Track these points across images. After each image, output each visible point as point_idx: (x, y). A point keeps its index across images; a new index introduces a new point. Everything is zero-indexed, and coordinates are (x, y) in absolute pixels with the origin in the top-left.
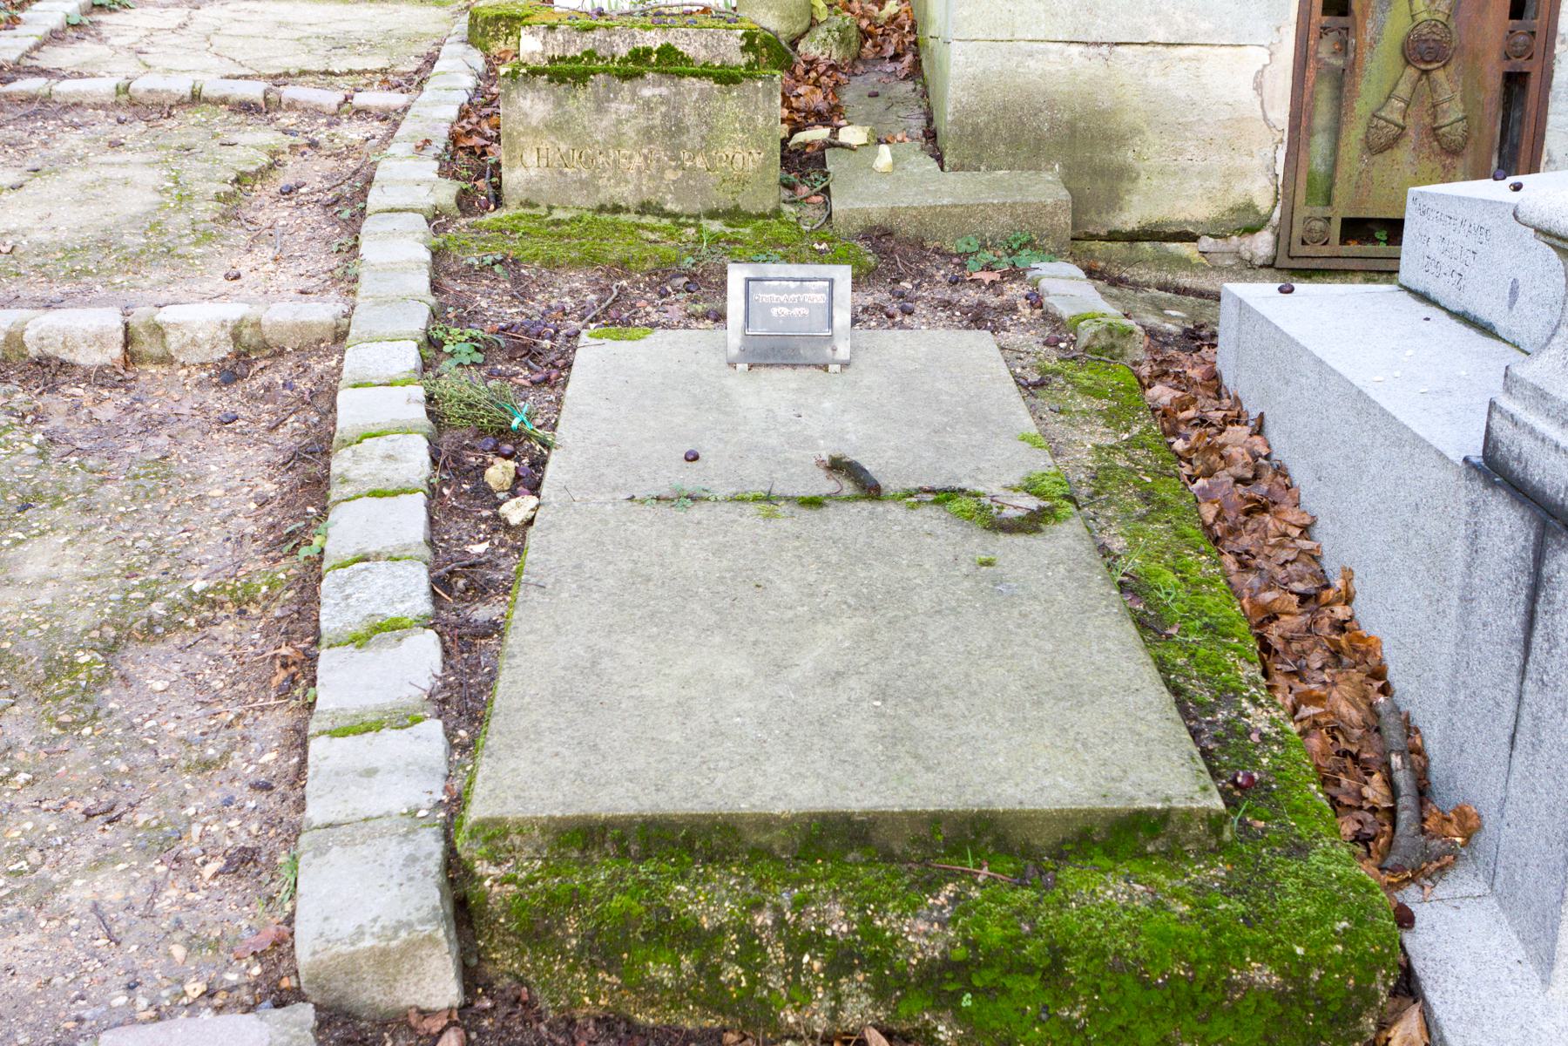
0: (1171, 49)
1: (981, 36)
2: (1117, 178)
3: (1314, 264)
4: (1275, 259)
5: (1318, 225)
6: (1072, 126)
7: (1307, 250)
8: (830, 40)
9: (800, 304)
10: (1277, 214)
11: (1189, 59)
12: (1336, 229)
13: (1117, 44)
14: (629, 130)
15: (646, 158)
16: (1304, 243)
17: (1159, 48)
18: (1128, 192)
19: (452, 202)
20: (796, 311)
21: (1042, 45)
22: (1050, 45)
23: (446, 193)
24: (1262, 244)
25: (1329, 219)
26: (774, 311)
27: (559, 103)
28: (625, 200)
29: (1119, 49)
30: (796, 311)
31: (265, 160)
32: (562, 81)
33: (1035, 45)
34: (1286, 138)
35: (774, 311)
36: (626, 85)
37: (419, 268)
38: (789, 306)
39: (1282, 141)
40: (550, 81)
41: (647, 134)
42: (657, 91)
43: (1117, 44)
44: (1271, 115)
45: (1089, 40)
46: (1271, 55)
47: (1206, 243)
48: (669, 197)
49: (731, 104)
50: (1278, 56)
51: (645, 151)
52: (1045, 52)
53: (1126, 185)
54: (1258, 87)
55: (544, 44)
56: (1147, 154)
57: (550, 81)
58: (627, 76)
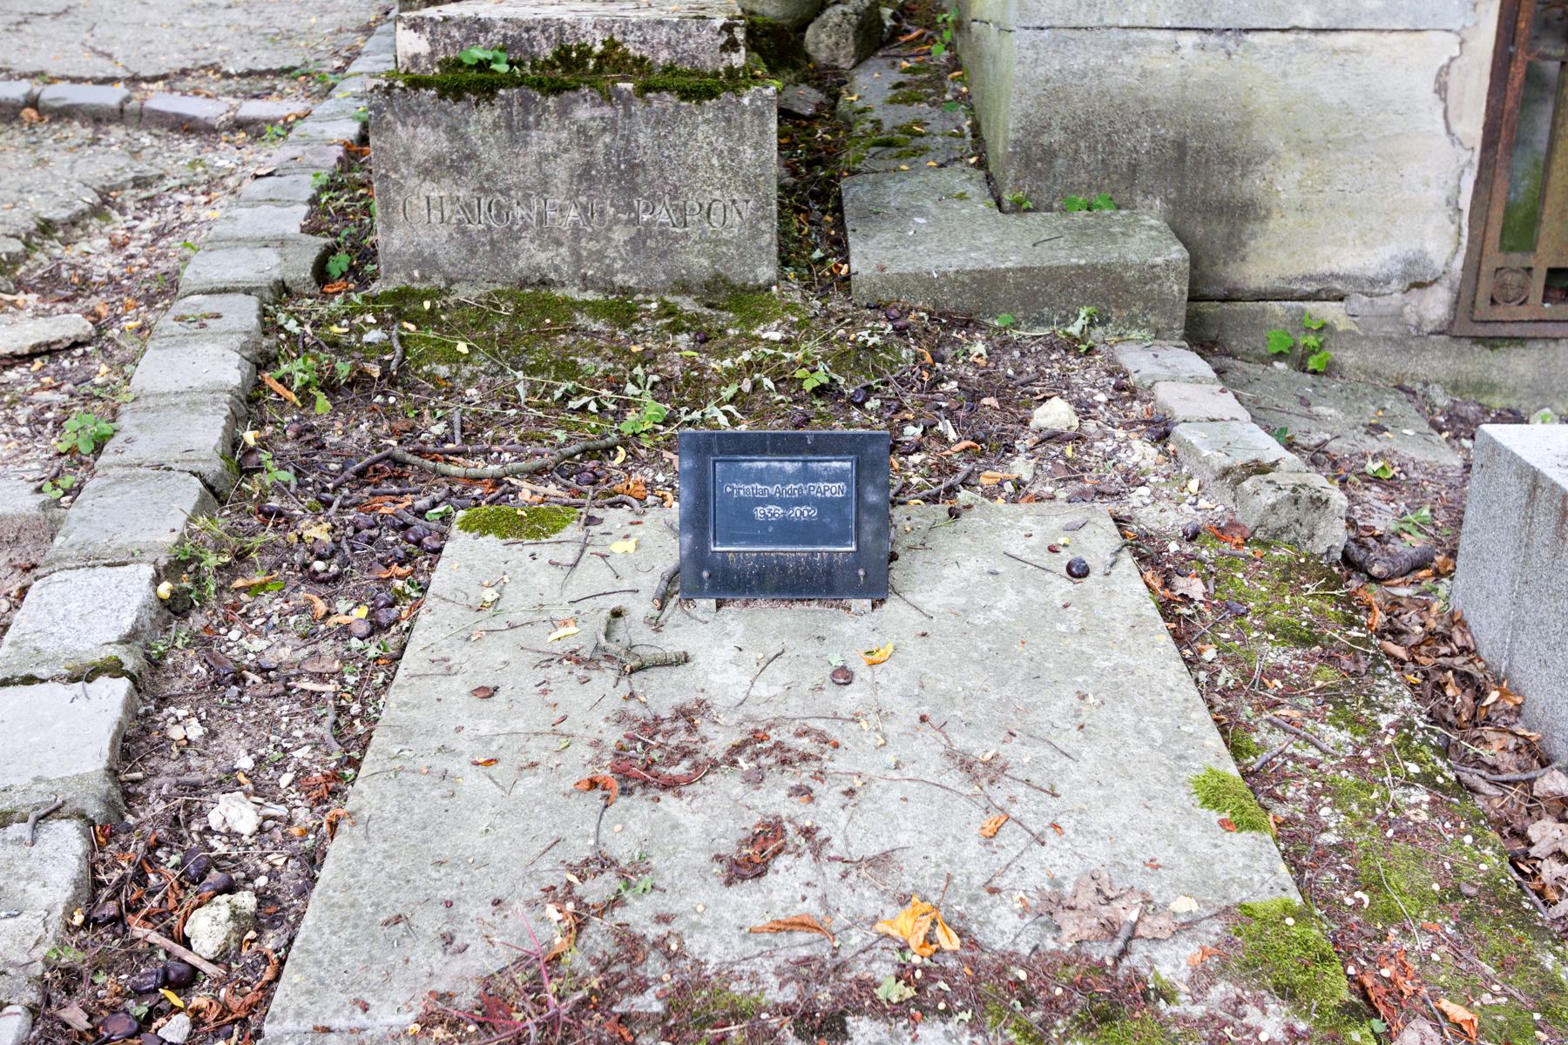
0: (1322, 37)
1: (1057, 23)
2: (1241, 214)
3: (1505, 331)
4: (1452, 323)
5: (1513, 279)
6: (1180, 146)
7: (1500, 312)
8: (846, 26)
9: (800, 502)
10: (1458, 263)
11: (1347, 51)
12: (1538, 284)
13: (1247, 31)
14: (560, 172)
15: (585, 209)
16: (1493, 302)
17: (1305, 36)
18: (1253, 235)
19: (307, 274)
20: (795, 512)
21: (1142, 34)
22: (1153, 34)
23: (300, 267)
24: (1435, 305)
25: (1529, 270)
26: (759, 512)
27: (453, 132)
28: (557, 269)
29: (1250, 37)
30: (795, 512)
31: (91, 198)
32: (458, 98)
33: (1134, 34)
34: (1476, 160)
35: (759, 512)
36: (551, 101)
37: (215, 401)
38: (786, 503)
39: (1470, 162)
40: (441, 96)
41: (584, 175)
42: (597, 112)
43: (1247, 31)
44: (1458, 128)
45: (1209, 25)
46: (1461, 44)
47: (1359, 303)
48: (618, 265)
49: (703, 130)
50: (1471, 44)
51: (583, 199)
52: (1144, 44)
53: (1252, 227)
54: (1441, 89)
55: (432, 42)
56: (1284, 181)
57: (441, 96)
58: (557, 89)
